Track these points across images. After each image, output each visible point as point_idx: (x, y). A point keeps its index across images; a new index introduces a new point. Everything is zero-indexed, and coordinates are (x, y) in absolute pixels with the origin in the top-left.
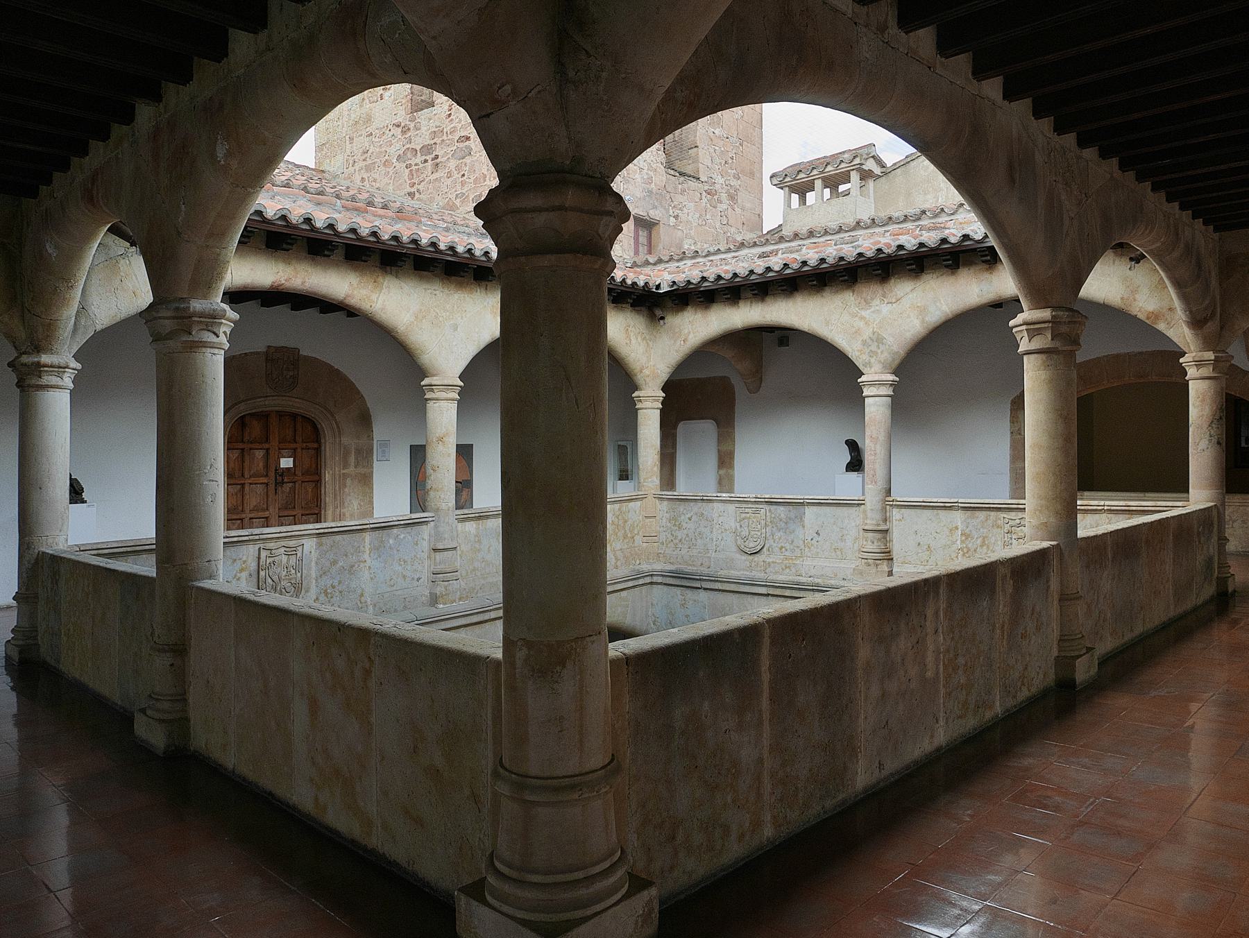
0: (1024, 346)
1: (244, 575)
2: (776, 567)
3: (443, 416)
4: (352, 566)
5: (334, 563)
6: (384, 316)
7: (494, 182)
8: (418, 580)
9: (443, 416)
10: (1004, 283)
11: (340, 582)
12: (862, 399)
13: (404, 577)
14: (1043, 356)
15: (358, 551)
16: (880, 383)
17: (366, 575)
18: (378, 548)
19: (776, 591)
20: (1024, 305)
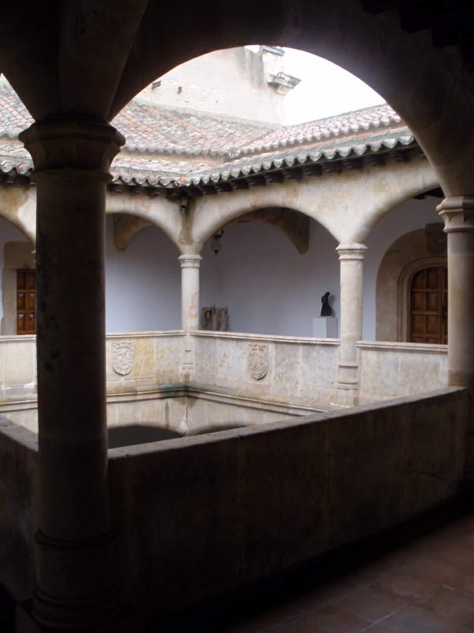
0: (448, 226)
1: (245, 356)
2: (273, 389)
3: (349, 272)
4: (292, 364)
5: (283, 360)
6: (263, 204)
7: (33, 121)
8: (332, 383)
9: (349, 272)
10: (425, 176)
11: (286, 372)
12: (338, 263)
13: (323, 379)
14: (460, 234)
15: (295, 356)
16: (351, 251)
17: (300, 372)
18: (306, 356)
19: (270, 407)
20: (446, 192)
